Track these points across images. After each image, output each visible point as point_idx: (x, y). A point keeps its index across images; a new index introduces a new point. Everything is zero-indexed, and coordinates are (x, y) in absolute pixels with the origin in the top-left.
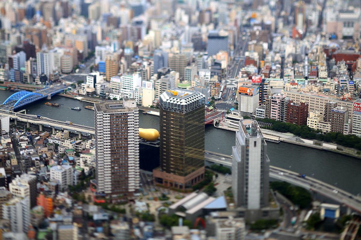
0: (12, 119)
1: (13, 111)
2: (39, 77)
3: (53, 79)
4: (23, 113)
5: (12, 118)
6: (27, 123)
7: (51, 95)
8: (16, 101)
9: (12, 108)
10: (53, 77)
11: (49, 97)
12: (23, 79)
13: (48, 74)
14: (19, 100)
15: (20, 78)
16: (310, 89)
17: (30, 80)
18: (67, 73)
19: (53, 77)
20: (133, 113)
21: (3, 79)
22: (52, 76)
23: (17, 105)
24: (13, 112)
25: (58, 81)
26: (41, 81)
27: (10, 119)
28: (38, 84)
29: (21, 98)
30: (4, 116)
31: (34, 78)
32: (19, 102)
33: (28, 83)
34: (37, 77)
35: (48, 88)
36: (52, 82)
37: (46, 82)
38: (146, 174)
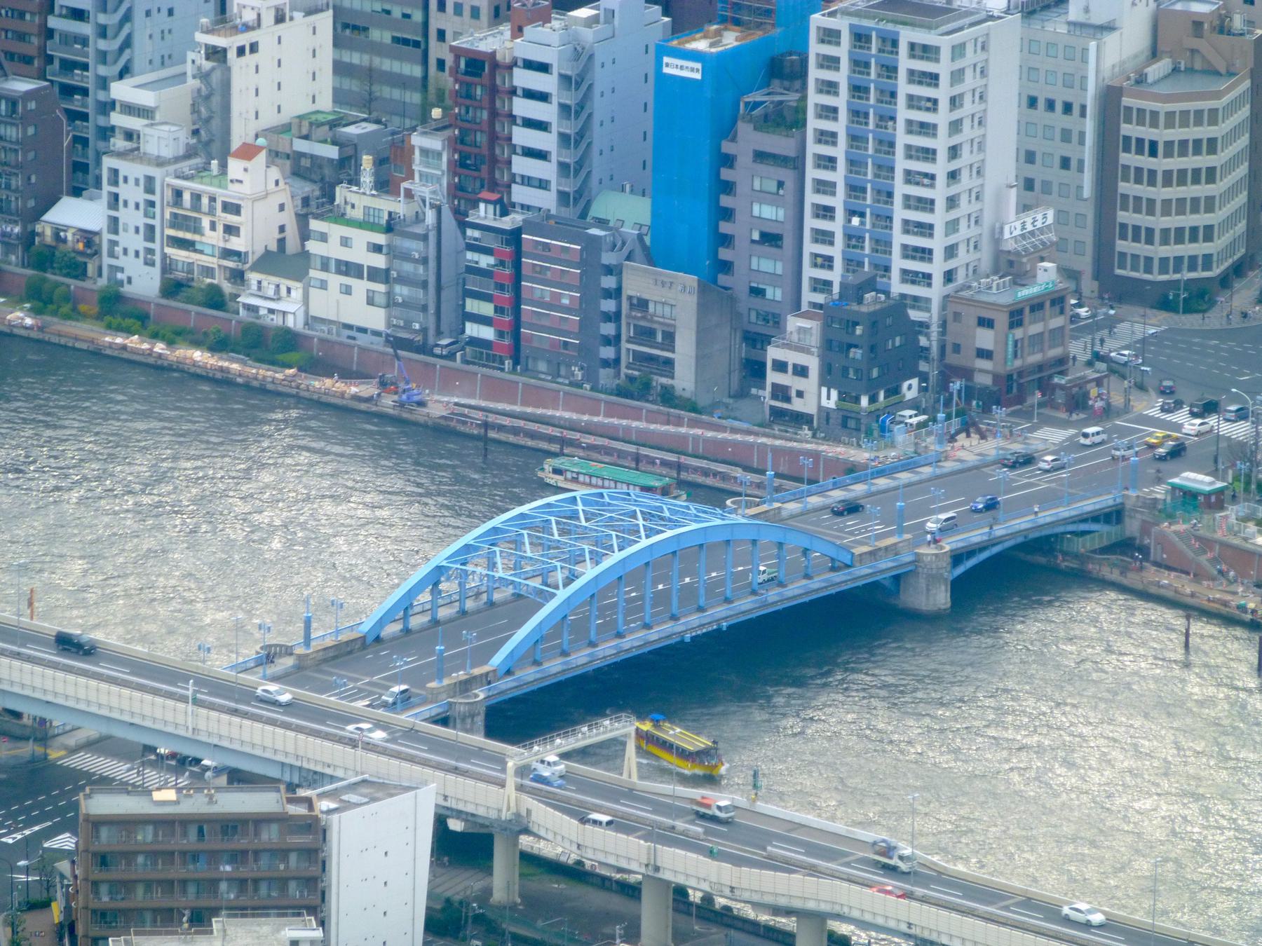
0: (455, 825)
1: (480, 721)
2: (813, 325)
3: (984, 354)
4: (608, 752)
5: (459, 814)
6: (647, 895)
7: (957, 558)
8: (522, 605)
9: (465, 686)
10: (985, 338)
11: (933, 578)
12: (615, 341)
13: (935, 292)
14: (562, 594)
15: (585, 307)
16: (1077, 757)
17: (702, 359)
18: (1164, 301)
19: (985, 338)
20: (872, 775)
21: (376, 319)
22: (986, 323)
23: (532, 653)
24: (478, 739)
25: (1044, 385)
26: (828, 377)
27: (440, 822)
28: (797, 405)
29: (589, 572)
30: (377, 789)
31: (757, 340)
32: (559, 624)
33: (668, 397)
34: (794, 323)
35: (927, 471)
36: (969, 392)
37: (894, 391)
38: (444, 563)
